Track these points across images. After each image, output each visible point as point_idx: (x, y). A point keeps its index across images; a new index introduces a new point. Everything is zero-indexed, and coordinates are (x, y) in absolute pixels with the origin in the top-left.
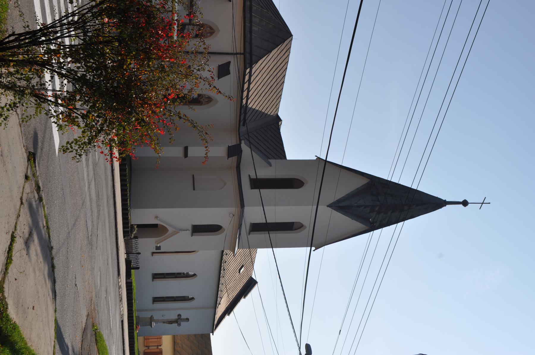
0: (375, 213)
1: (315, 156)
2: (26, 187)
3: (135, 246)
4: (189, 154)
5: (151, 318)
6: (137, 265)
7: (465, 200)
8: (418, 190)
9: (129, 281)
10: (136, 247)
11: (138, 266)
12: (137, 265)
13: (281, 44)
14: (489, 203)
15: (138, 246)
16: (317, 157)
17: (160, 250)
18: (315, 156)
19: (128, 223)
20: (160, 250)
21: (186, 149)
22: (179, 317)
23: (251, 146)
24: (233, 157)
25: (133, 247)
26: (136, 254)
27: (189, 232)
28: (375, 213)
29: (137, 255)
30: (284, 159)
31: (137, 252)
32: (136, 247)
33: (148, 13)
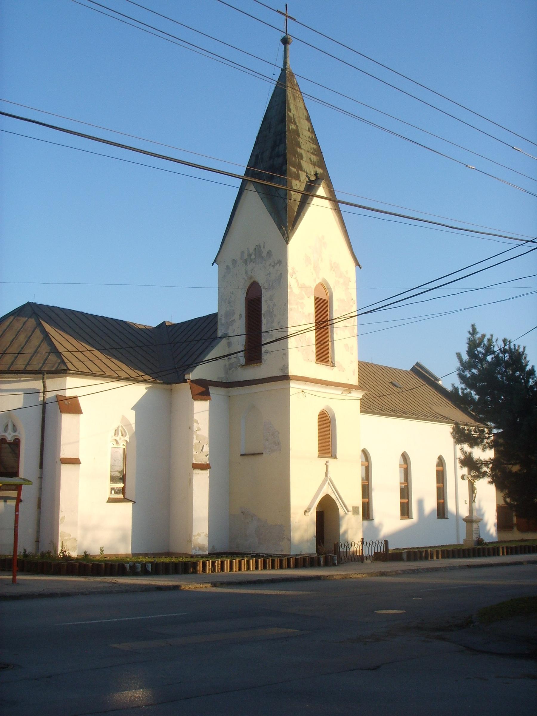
0: (300, 171)
1: (213, 265)
2: (13, 486)
3: (368, 546)
4: (197, 471)
5: (466, 522)
6: (380, 544)
7: (281, 40)
8: (240, 187)
9: (405, 556)
10: (345, 545)
11: (383, 542)
12: (380, 544)
13: (48, 334)
14: (286, 5)
15: (374, 542)
16: (214, 263)
17: (358, 507)
18: (213, 265)
19: (474, 549)
20: (358, 507)
21: (196, 466)
22: (465, 477)
23: (196, 362)
24: (210, 393)
25: (345, 550)
26: (364, 546)
27: (331, 461)
28: (300, 171)
29: (365, 543)
30: (217, 315)
31: (360, 543)
32: (345, 545)
33: (91, 564)
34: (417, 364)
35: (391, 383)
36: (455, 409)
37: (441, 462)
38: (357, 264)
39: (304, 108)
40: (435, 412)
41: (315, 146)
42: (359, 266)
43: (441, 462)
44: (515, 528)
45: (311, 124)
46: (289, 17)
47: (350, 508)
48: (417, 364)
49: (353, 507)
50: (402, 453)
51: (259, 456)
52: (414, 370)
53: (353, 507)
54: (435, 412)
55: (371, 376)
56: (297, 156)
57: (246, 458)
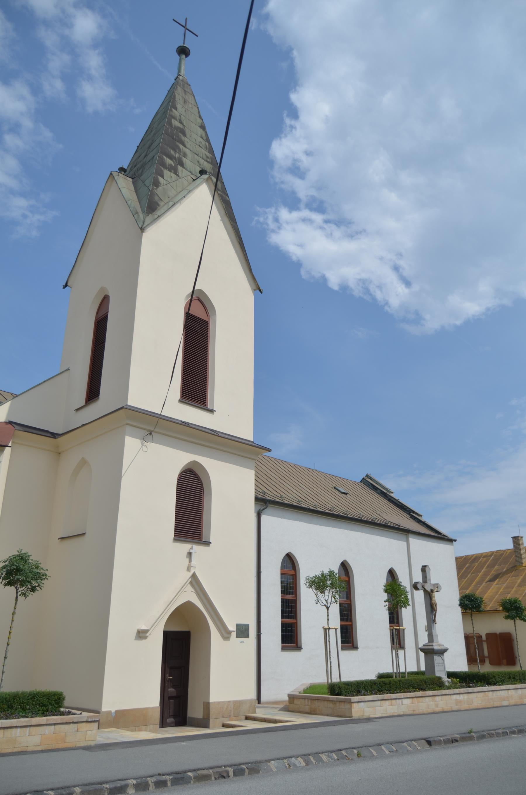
27: (197, 549)
34: (367, 476)
35: (335, 488)
36: (409, 519)
37: (270, 450)
38: (258, 289)
39: (198, 116)
40: (384, 519)
41: (209, 155)
42: (260, 290)
43: (270, 450)
44: (258, 634)
45: (206, 132)
46: (187, 29)
47: (232, 627)
48: (367, 476)
49: (238, 625)
50: (341, 562)
51: (80, 539)
52: (363, 481)
53: (238, 625)
54: (384, 519)
55: (309, 475)
56: (177, 151)
57: (67, 542)
